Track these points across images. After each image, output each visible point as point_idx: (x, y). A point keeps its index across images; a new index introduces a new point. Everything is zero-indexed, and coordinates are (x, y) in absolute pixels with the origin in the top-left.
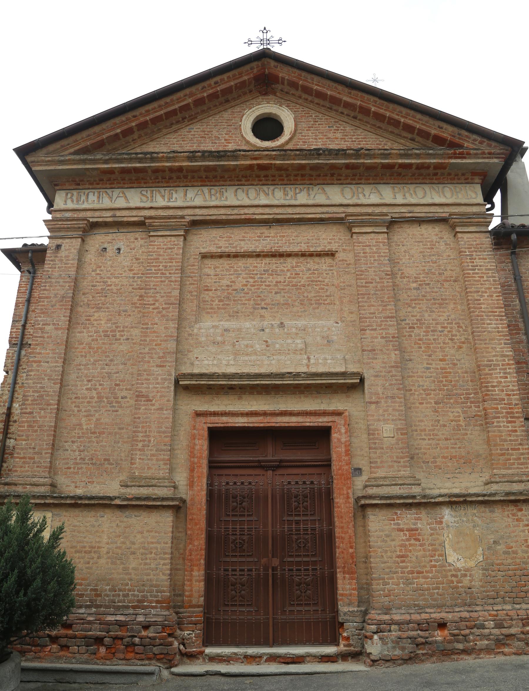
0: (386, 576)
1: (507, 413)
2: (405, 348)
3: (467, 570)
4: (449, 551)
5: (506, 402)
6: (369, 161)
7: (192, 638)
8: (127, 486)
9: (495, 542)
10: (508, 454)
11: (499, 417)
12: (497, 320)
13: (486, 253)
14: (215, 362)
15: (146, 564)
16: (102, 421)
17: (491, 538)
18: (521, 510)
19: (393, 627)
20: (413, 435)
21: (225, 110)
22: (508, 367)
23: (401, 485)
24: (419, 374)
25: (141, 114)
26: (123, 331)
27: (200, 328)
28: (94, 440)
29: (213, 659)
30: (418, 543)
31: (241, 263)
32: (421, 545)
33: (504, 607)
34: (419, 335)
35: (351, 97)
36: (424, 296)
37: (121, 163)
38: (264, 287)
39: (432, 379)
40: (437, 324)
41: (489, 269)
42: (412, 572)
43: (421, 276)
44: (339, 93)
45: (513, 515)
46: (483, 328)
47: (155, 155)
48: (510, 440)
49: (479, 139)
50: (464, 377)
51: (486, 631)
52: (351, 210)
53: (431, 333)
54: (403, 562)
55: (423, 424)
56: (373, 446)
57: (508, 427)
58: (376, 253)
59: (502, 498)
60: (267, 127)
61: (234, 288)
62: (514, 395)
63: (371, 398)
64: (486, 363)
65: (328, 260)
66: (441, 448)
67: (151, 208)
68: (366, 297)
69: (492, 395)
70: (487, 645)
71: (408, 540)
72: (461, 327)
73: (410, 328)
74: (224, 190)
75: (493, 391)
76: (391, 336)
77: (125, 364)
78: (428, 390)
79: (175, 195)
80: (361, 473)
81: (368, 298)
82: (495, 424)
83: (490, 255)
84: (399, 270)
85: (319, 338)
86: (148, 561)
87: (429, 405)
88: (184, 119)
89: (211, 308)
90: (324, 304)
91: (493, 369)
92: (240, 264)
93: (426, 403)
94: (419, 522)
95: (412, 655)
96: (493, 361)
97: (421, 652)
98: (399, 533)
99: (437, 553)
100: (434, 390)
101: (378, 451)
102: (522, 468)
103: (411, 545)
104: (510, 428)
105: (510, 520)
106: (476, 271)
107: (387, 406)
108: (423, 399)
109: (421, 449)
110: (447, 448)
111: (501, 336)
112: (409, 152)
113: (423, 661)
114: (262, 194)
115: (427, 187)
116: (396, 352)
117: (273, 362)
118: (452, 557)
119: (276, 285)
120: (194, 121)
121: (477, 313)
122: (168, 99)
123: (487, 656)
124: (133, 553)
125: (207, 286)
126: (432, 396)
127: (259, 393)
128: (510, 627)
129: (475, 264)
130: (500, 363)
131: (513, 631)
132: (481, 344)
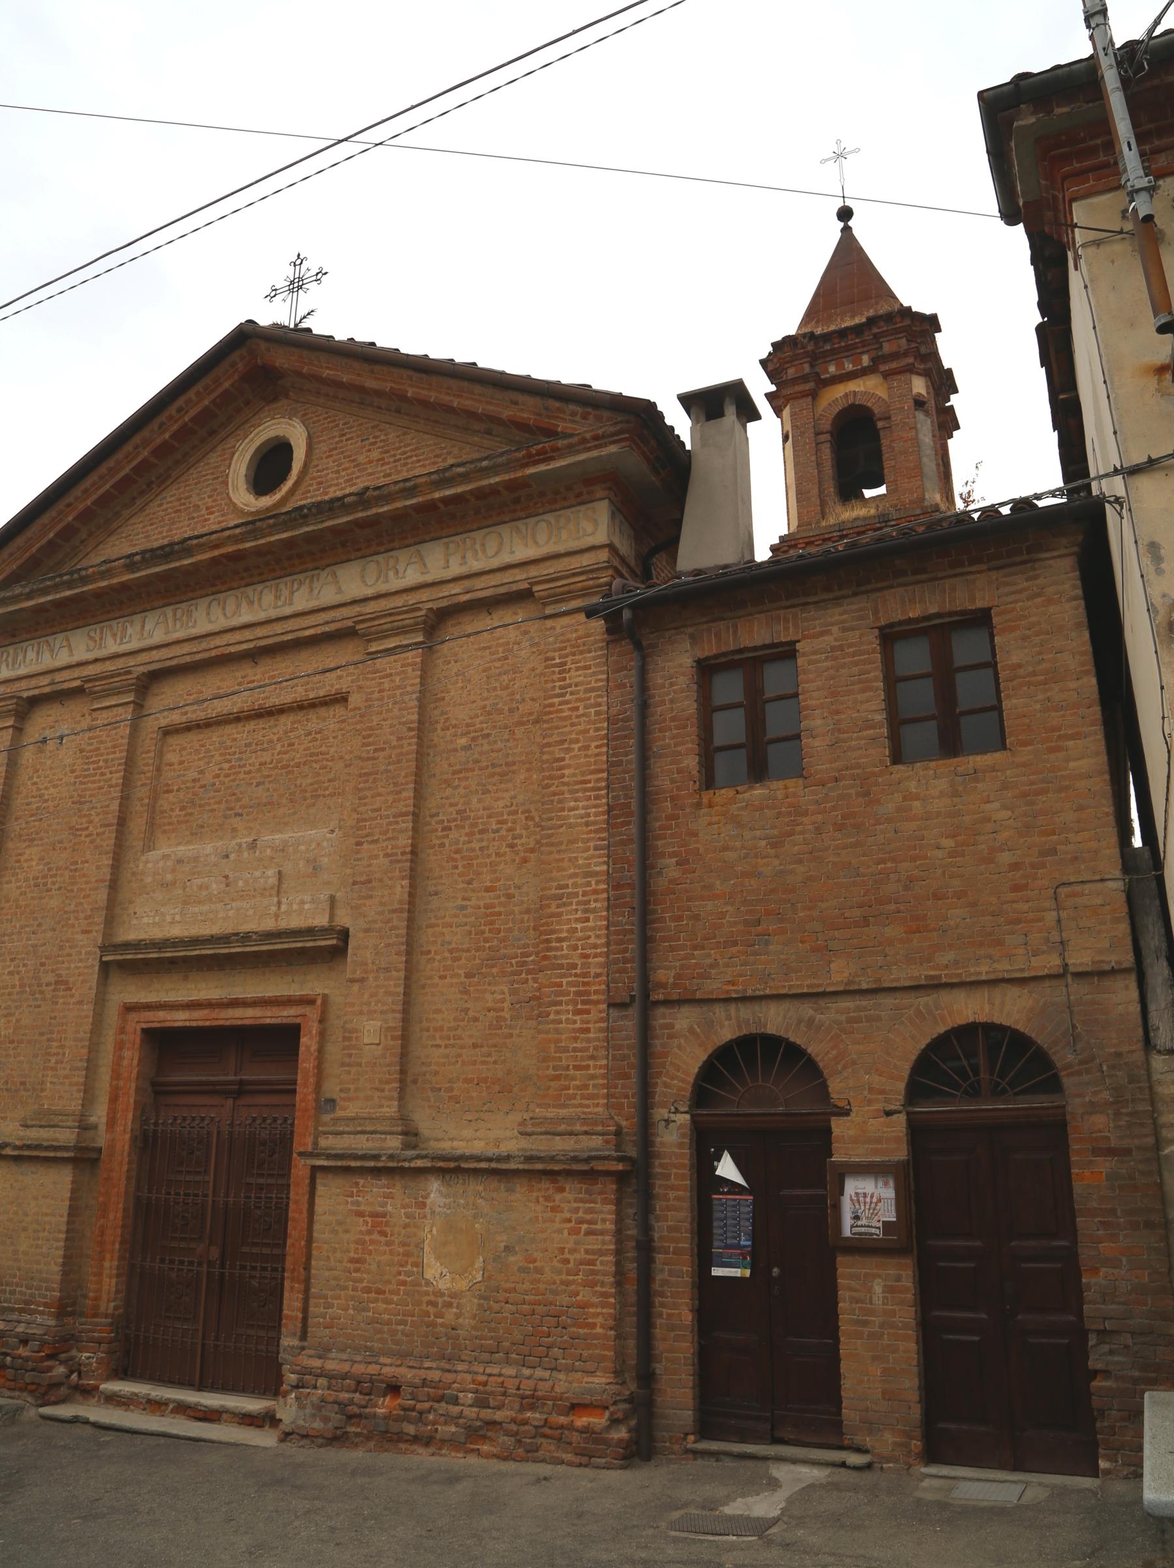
0: (330, 1293)
1: (578, 993)
2: (431, 870)
3: (454, 1295)
4: (429, 1258)
5: (578, 971)
6: (385, 509)
7: (91, 1364)
8: (27, 1126)
9: (507, 1248)
10: (567, 1077)
11: (560, 1003)
12: (589, 798)
13: (593, 654)
14: (157, 919)
15: (37, 1246)
16: (23, 1023)
17: (502, 1240)
18: (562, 1190)
19: (322, 1382)
20: (421, 1038)
21: (213, 449)
22: (593, 897)
23: (372, 1133)
24: (447, 920)
25: (76, 499)
26: (56, 875)
27: (147, 862)
28: (11, 1052)
29: (112, 1399)
30: (383, 1239)
31: (215, 737)
32: (388, 1244)
33: (503, 1371)
34: (457, 842)
35: (377, 379)
36: (477, 761)
37: (48, 593)
38: (242, 776)
39: (467, 928)
40: (489, 817)
41: (592, 690)
42: (368, 1290)
43: (477, 720)
44: (359, 375)
45: (547, 1199)
46: (559, 818)
47: (84, 573)
48: (575, 1050)
49: (579, 409)
50: (522, 921)
51: (455, 1410)
52: (371, 607)
53: (478, 836)
54: (357, 1270)
55: (439, 1017)
56: (347, 1060)
57: (575, 1022)
58: (399, 687)
59: (521, 1167)
60: (271, 466)
61: (202, 783)
62: (596, 956)
63: (354, 972)
64: (553, 891)
65: (339, 710)
66: (464, 1063)
67: (96, 660)
68: (371, 779)
69: (555, 957)
70: (453, 1434)
71: (369, 1233)
72: (532, 819)
73: (443, 829)
74: (193, 608)
75: (557, 949)
76: (399, 851)
77: (54, 930)
78: (457, 950)
79: (129, 631)
80: (334, 1106)
81: (375, 780)
82: (552, 1017)
83: (598, 657)
84: (443, 713)
85: (301, 864)
86: (40, 1242)
87: (455, 980)
88: (150, 484)
89: (170, 824)
90: (324, 796)
91: (565, 905)
92: (215, 739)
93: (452, 977)
94: (389, 1201)
95: (338, 1432)
96: (567, 886)
97: (352, 1429)
98: (357, 1219)
99: (410, 1260)
100: (468, 951)
101: (354, 1070)
102: (588, 1106)
103: (372, 1242)
104: (578, 1025)
105: (539, 1208)
106: (568, 697)
107: (377, 986)
108: (446, 968)
109: (430, 1064)
110: (475, 1062)
111: (590, 832)
112: (447, 474)
113: (356, 1445)
114: (244, 604)
115: (505, 530)
116: (403, 883)
117: (231, 913)
118: (434, 1270)
119: (259, 770)
120: (168, 483)
121: (553, 789)
122: (111, 463)
123: (453, 1454)
124: (25, 1229)
125: (168, 785)
126: (463, 961)
127: (210, 969)
128: (498, 1408)
129: (568, 681)
130: (580, 890)
131: (498, 1416)
132: (551, 853)
